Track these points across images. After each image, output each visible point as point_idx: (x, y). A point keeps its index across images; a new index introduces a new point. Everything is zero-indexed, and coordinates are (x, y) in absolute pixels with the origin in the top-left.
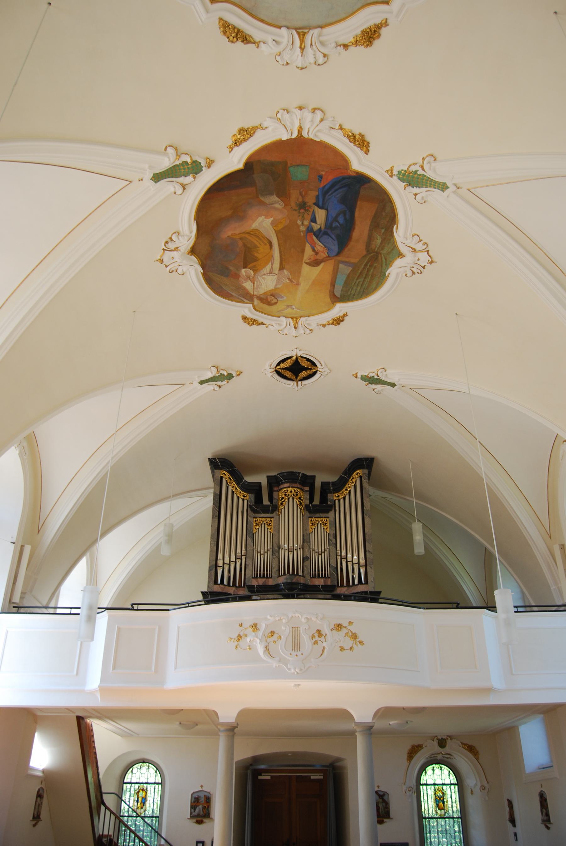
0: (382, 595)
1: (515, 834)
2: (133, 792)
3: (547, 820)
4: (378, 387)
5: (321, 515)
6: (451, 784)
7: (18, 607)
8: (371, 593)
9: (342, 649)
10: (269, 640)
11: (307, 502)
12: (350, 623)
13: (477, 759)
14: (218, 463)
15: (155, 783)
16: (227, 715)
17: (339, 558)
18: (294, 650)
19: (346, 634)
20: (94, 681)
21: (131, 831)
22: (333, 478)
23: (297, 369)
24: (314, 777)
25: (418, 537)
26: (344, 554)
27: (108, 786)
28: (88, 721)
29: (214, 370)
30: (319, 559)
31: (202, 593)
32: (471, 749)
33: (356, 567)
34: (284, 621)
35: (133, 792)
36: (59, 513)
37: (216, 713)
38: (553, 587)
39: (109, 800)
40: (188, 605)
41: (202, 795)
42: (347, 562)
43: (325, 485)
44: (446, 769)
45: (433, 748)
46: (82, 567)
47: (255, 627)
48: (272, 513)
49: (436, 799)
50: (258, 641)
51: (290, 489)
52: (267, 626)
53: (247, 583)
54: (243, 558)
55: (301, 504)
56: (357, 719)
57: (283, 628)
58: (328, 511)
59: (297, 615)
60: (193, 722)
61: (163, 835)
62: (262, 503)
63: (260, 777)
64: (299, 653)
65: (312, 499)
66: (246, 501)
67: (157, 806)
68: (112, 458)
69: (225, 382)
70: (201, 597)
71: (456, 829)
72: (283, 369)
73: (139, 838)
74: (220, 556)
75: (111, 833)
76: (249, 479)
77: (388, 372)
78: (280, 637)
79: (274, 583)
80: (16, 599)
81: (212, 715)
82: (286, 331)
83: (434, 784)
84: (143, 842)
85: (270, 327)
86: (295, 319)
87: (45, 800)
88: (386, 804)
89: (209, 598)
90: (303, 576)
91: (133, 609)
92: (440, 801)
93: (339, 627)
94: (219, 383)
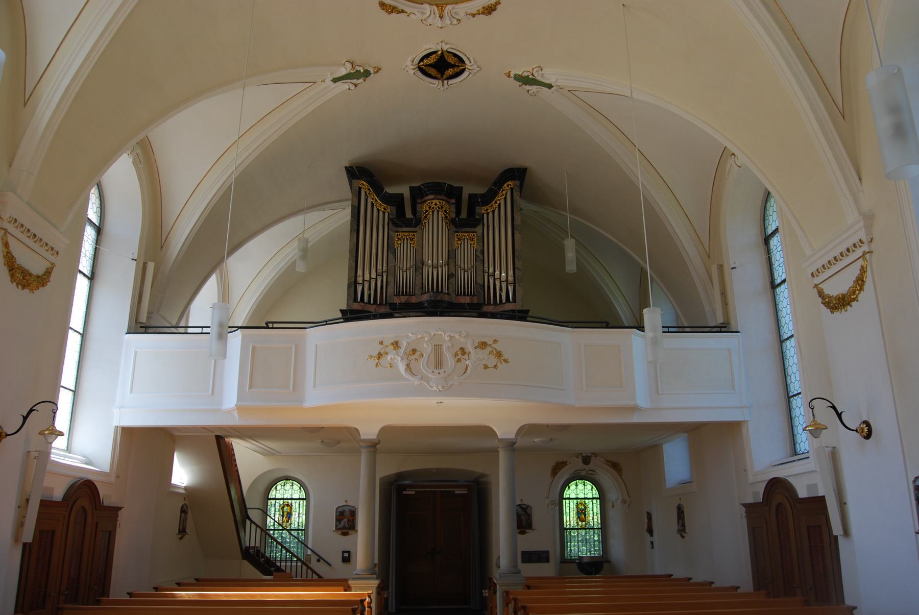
0: (530, 314)
1: (652, 543)
2: (277, 507)
3: (682, 530)
4: (533, 88)
5: (468, 229)
6: (593, 498)
7: (146, 327)
8: (519, 311)
9: (486, 367)
10: (410, 358)
11: (453, 215)
12: (495, 341)
13: (620, 475)
14: (356, 172)
15: (299, 499)
16: (369, 431)
17: (486, 275)
18: (436, 368)
19: (490, 352)
20: (230, 400)
21: (278, 542)
22: (481, 190)
23: (442, 66)
24: (458, 492)
25: (570, 255)
26: (491, 271)
27: (252, 502)
28: (227, 440)
29: (348, 65)
30: (465, 277)
31: (341, 311)
32: (615, 466)
33: (504, 285)
34: (426, 339)
35: (277, 507)
36: (183, 228)
37: (357, 430)
38: (707, 308)
39: (254, 515)
40: (326, 323)
41: (346, 509)
42: (494, 279)
43: (471, 196)
44: (589, 485)
45: (578, 464)
46: (212, 283)
47: (396, 345)
48: (415, 227)
49: (578, 512)
50: (399, 359)
51: (434, 202)
52: (408, 344)
53: (389, 301)
54: (385, 274)
55: (446, 217)
56: (500, 435)
57: (425, 346)
58: (475, 226)
59: (440, 333)
60: (333, 440)
61: (310, 546)
62: (404, 216)
63: (404, 492)
64: (442, 371)
65: (458, 212)
66: (386, 214)
67: (303, 519)
68: (236, 168)
69: (361, 81)
70: (340, 316)
71: (596, 539)
72: (426, 65)
73: (285, 548)
74: (360, 272)
75: (258, 545)
76: (391, 190)
77: (546, 71)
78: (422, 355)
79: (418, 301)
80: (143, 319)
81: (353, 432)
82: (430, 21)
83: (577, 498)
84: (290, 552)
85: (412, 16)
86: (441, 7)
87: (189, 515)
88: (529, 516)
89: (349, 316)
90: (448, 294)
91: (268, 328)
92: (582, 513)
93: (483, 345)
94: (355, 81)
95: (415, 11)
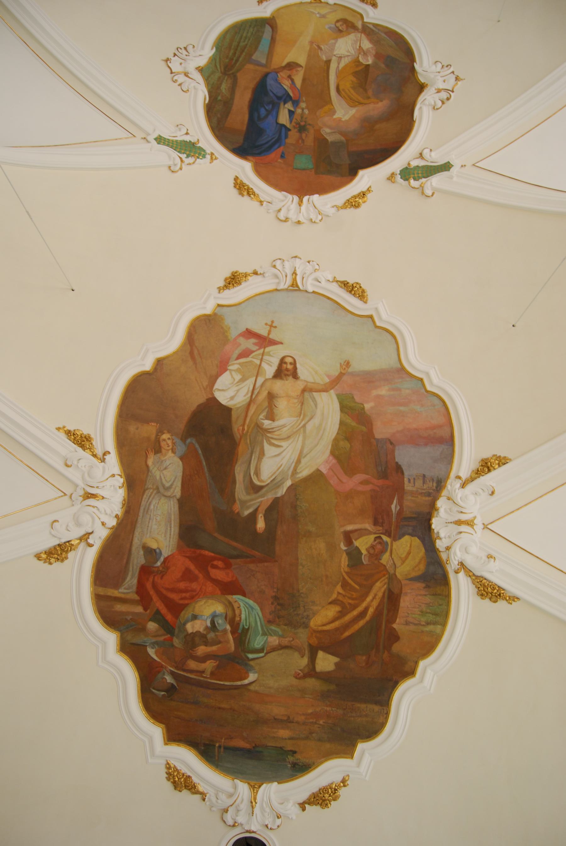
4: (180, 137)
82: (309, 268)
94: (421, 163)
95: (324, 284)
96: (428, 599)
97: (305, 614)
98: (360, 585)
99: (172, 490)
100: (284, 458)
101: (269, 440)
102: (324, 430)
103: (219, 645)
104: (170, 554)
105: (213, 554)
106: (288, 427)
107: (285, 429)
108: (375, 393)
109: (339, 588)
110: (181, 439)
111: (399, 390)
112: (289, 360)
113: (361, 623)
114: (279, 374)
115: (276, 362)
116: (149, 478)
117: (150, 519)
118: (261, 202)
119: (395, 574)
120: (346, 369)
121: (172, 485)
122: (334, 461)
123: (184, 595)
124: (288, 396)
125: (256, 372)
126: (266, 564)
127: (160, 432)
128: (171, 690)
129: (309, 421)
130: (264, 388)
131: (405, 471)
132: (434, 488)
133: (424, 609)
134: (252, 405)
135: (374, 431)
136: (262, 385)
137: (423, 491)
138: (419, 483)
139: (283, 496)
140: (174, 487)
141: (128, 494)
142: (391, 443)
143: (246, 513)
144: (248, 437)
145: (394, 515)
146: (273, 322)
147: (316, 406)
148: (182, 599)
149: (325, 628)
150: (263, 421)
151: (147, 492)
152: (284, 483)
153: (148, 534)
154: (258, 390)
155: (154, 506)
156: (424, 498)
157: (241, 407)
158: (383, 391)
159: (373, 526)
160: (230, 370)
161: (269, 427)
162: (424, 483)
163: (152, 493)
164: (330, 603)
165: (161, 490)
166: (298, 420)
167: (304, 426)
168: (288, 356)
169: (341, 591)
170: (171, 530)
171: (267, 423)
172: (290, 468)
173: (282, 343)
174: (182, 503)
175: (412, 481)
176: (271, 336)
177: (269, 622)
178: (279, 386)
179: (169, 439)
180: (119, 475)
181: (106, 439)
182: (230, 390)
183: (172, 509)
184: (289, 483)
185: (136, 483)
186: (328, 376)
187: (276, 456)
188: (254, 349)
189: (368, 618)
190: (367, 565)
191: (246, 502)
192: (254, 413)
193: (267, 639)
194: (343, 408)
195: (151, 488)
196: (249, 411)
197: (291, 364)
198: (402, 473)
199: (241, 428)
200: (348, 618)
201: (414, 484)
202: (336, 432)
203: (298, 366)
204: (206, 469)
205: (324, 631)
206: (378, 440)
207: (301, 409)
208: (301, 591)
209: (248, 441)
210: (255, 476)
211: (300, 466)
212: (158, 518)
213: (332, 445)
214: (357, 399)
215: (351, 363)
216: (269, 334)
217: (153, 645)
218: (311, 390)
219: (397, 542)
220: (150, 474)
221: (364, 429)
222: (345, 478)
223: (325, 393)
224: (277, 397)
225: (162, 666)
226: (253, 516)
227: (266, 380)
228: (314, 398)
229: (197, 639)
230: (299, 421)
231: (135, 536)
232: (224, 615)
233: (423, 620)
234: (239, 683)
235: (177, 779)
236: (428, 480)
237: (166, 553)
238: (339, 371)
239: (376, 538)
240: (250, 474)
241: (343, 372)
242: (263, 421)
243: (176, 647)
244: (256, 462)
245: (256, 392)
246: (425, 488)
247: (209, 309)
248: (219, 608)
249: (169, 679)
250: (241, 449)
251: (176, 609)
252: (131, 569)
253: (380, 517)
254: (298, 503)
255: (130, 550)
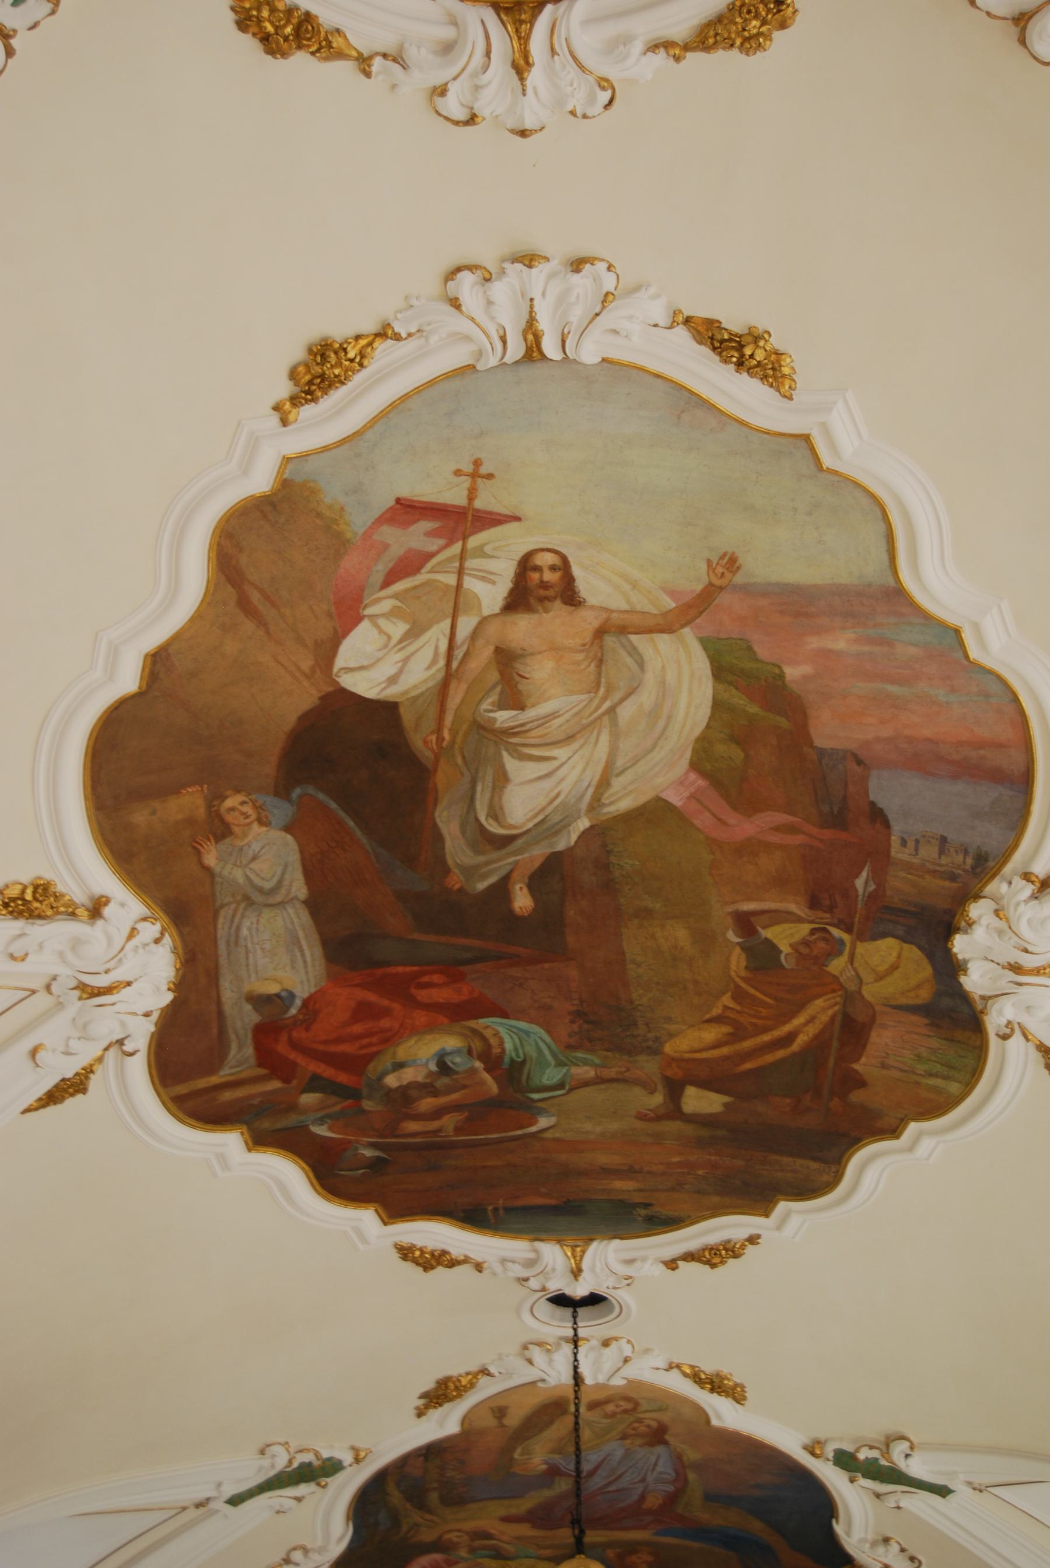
96: (934, 1043)
97: (651, 1035)
98: (776, 999)
99: (283, 891)
100: (562, 780)
101: (516, 751)
102: (669, 718)
103: (463, 1091)
104: (313, 990)
105: (415, 968)
106: (567, 716)
107: (557, 722)
108: (814, 643)
109: (727, 1000)
110: (276, 794)
111: (890, 644)
112: (546, 560)
113: (781, 1054)
114: (523, 596)
115: (505, 570)
116: (218, 888)
117: (247, 953)
118: (364, 63)
119: (859, 993)
120: (728, 575)
121: (280, 882)
122: (701, 782)
123: (365, 1041)
124: (555, 649)
125: (452, 604)
126: (546, 966)
127: (216, 797)
128: (376, 1165)
129: (622, 700)
130: (480, 642)
131: (892, 823)
132: (968, 867)
133: (924, 1055)
134: (453, 684)
135: (813, 732)
136: (474, 635)
137: (938, 868)
138: (929, 852)
139: (570, 850)
140: (286, 883)
141: (181, 934)
142: (859, 762)
143: (481, 886)
144: (457, 752)
145: (860, 898)
146: (477, 463)
147: (641, 664)
148: (362, 1047)
149: (698, 1056)
150: (492, 715)
151: (222, 913)
152: (570, 825)
153: (253, 976)
154: (465, 648)
155: (250, 929)
156: (939, 882)
157: (422, 694)
158: (841, 642)
159: (806, 910)
160: (372, 617)
161: (512, 724)
162: (942, 852)
163: (236, 910)
164: (709, 1021)
165: (253, 899)
166: (591, 700)
167: (612, 710)
168: (543, 550)
169: (732, 1004)
170: (303, 955)
171: (503, 717)
172: (582, 797)
173: (518, 519)
174: (314, 906)
175: (911, 844)
176: (478, 504)
177: (570, 1047)
178: (523, 629)
179: (243, 803)
180: (145, 919)
181: (85, 867)
182: (381, 661)
183: (295, 920)
184: (584, 824)
185: (189, 911)
186: (672, 594)
187: (540, 778)
188: (434, 548)
189: (795, 1047)
190: (792, 969)
191: (477, 867)
192: (462, 701)
193: (568, 1071)
194: (720, 672)
195: (229, 904)
196: (449, 699)
197: (553, 568)
198: (887, 825)
199: (434, 738)
200: (748, 1044)
201: (917, 849)
202: (704, 724)
203: (576, 571)
204: (358, 833)
205: (695, 1060)
206: (822, 752)
207: (599, 674)
208: (637, 1003)
209: (459, 760)
210: (491, 821)
211: (611, 791)
212: (267, 946)
213: (695, 751)
214: (762, 652)
215: (740, 561)
216: (471, 499)
217: (321, 1121)
218: (623, 630)
219: (865, 944)
220: (219, 880)
221: (783, 722)
222: (732, 818)
223: (666, 636)
224: (523, 656)
225: (349, 1142)
226: (502, 890)
227: (484, 621)
228: (635, 648)
229: (414, 1093)
230: (596, 702)
231: (222, 988)
232: (465, 1050)
233: (921, 1068)
234: (519, 1132)
235: (270, 28)
236: (952, 850)
237: (302, 991)
238: (705, 580)
239: (813, 931)
240: (477, 819)
241: (717, 582)
242: (492, 715)
243: (370, 1112)
244: (487, 795)
245: (459, 654)
246: (943, 862)
247: (260, 481)
248: (451, 1042)
249: (368, 1153)
250: (440, 779)
251: (357, 1064)
252: (233, 1037)
253: (824, 895)
254: (613, 859)
255: (220, 1014)
